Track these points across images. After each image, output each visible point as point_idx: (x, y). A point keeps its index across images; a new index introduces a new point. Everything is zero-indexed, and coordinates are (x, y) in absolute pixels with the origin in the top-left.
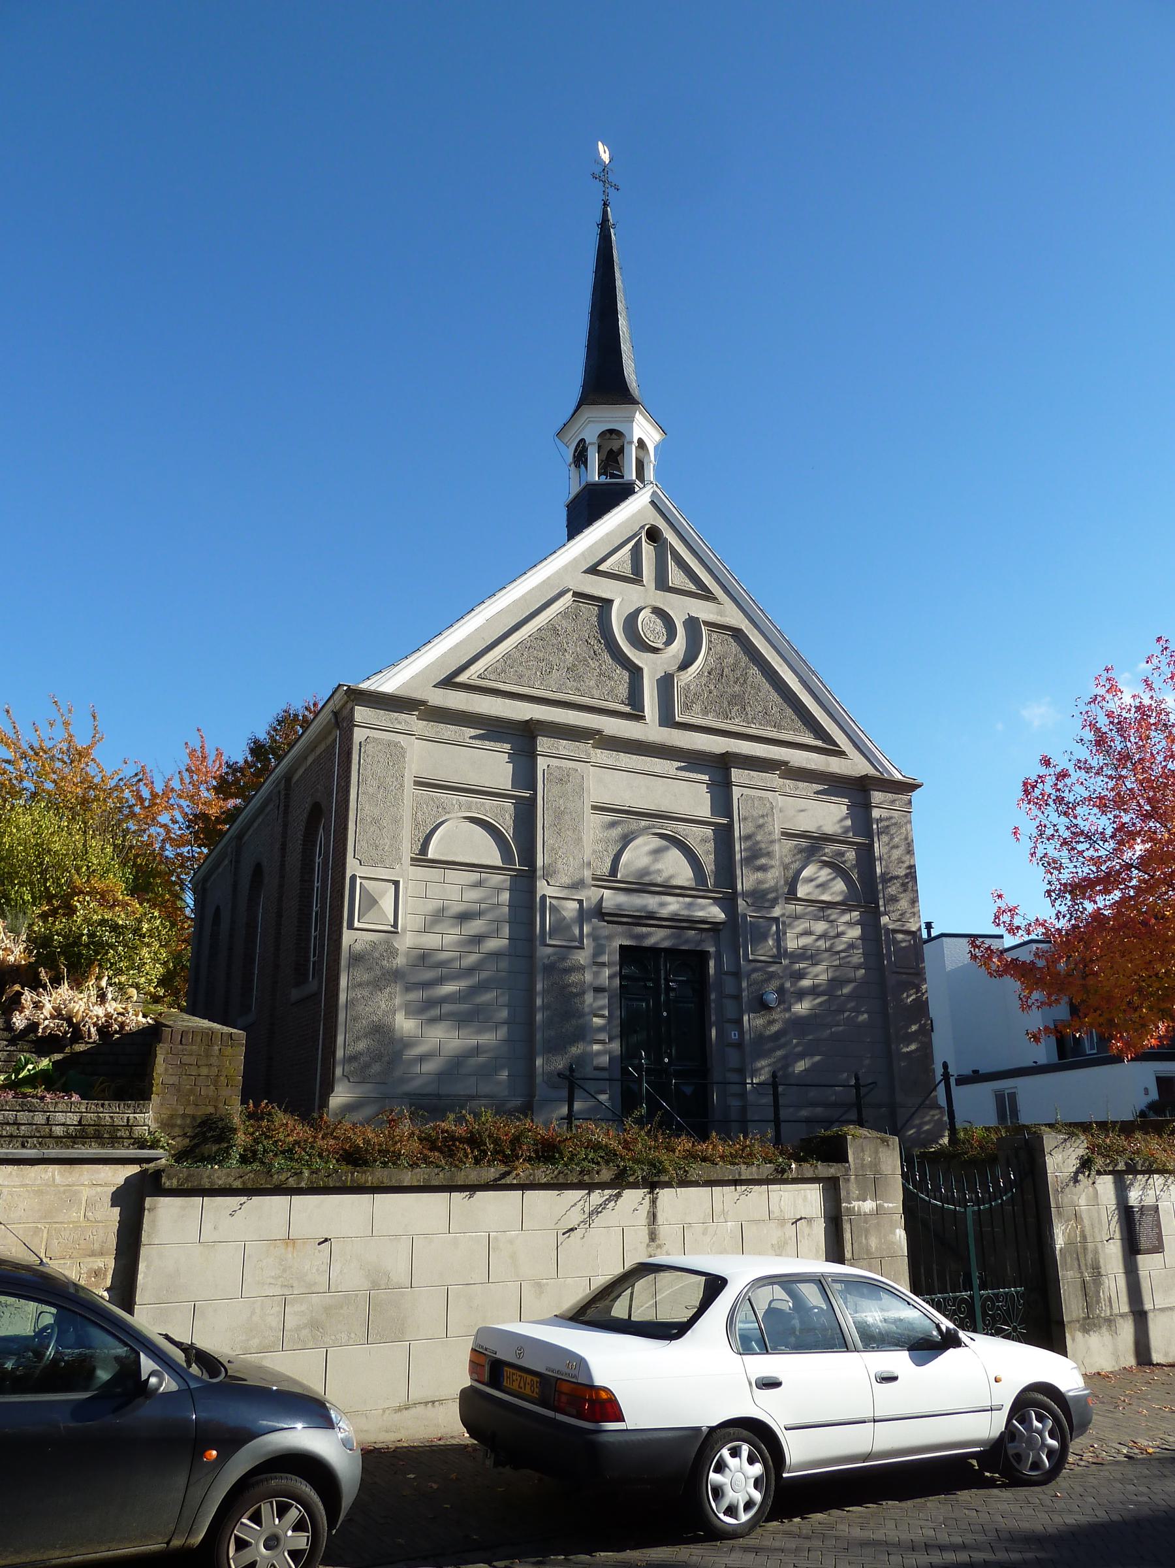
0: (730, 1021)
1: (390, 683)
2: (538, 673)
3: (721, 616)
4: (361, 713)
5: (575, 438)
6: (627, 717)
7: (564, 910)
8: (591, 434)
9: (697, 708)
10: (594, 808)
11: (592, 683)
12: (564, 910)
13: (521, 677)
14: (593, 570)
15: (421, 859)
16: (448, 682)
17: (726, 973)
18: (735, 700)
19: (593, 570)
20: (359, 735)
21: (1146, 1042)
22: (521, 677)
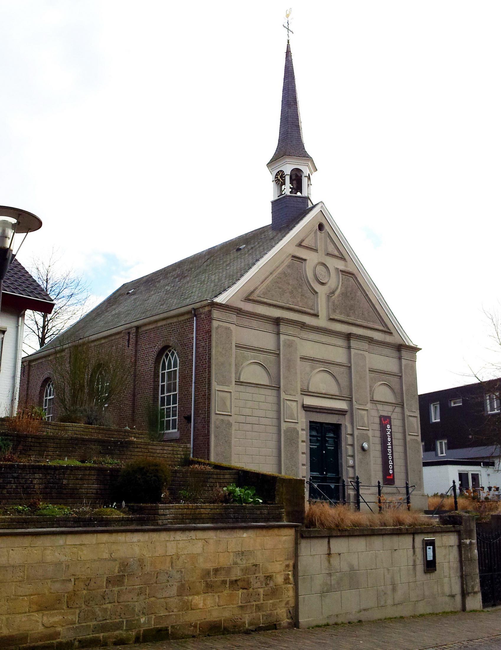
0: (349, 456)
1: (221, 299)
2: (279, 294)
3: (346, 267)
4: (216, 314)
5: (278, 168)
6: (342, 322)
7: (69, 465)
8: (288, 169)
9: (338, 311)
10: (301, 358)
11: (299, 299)
12: (69, 465)
13: (273, 296)
14: (300, 245)
15: (239, 383)
16: (248, 299)
17: (348, 434)
18: (352, 308)
19: (300, 245)
20: (215, 324)
21: (497, 394)
22: (273, 296)
